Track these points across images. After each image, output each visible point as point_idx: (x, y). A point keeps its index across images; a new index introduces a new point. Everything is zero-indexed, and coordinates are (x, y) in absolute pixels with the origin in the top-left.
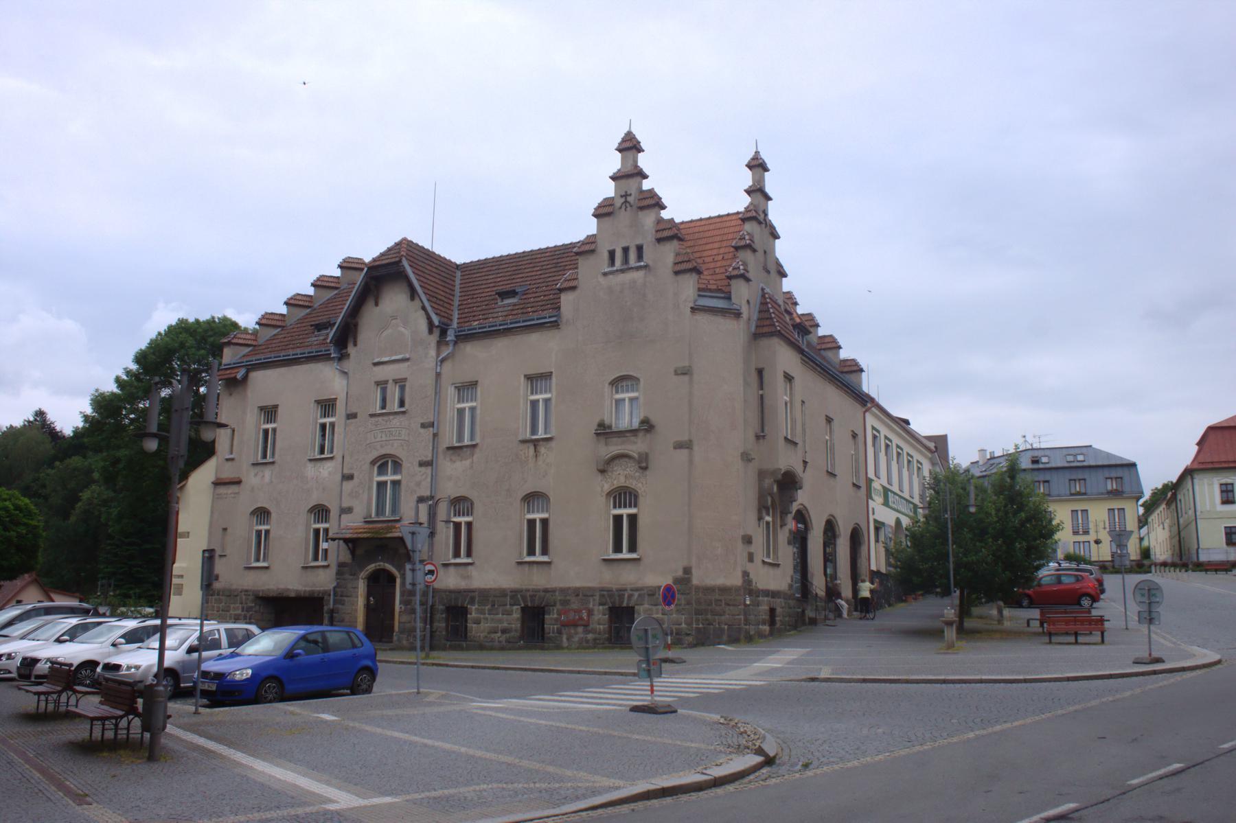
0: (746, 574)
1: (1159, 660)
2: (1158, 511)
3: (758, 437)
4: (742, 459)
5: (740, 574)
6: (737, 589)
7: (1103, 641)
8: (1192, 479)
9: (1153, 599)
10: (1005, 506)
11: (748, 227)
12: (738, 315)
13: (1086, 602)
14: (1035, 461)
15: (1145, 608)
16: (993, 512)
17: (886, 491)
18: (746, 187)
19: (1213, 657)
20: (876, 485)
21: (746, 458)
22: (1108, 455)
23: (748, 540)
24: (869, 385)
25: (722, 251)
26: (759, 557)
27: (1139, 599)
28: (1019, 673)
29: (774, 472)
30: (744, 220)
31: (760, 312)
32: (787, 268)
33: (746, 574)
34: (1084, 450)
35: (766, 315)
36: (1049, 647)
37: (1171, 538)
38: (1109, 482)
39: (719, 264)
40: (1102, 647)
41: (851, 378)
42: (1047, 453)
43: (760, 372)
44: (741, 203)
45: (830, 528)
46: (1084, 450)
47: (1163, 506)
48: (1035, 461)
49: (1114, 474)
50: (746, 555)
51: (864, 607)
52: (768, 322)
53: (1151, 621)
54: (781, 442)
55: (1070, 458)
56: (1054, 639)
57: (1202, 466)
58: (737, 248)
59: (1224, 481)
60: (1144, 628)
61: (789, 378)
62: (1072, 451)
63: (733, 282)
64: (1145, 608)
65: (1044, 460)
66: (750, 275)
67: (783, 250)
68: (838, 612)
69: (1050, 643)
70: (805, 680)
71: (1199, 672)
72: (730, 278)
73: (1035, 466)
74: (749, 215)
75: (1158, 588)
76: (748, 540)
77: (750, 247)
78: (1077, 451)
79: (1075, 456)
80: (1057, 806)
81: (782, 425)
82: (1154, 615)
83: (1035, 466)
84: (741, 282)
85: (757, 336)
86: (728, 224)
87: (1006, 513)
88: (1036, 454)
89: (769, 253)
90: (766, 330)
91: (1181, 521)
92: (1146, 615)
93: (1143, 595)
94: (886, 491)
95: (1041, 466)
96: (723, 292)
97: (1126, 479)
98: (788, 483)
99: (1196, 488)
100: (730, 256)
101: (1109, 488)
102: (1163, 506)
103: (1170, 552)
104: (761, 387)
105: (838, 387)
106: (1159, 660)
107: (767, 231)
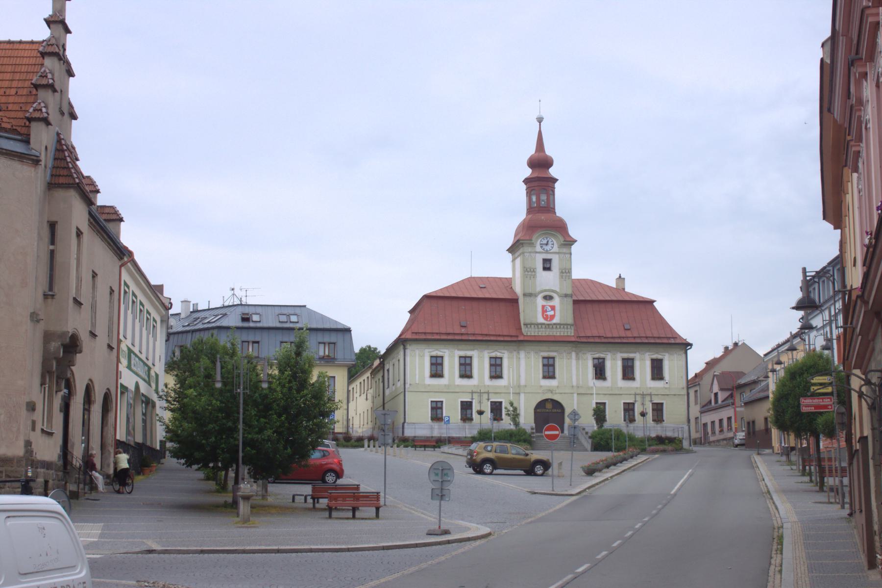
0: (28, 444)
1: (446, 532)
2: (361, 380)
3: (46, 296)
4: (32, 320)
5: (22, 443)
6: (19, 460)
7: (354, 517)
8: (405, 349)
9: (446, 478)
10: (290, 382)
11: (49, 62)
12: (36, 162)
13: (330, 478)
14: (246, 319)
15: (437, 486)
16: (279, 389)
17: (130, 351)
18: (46, 16)
19: (485, 530)
20: (123, 347)
21: (35, 318)
22: (323, 317)
23: (31, 407)
24: (127, 236)
25: (15, 84)
26: (39, 427)
27: (433, 477)
28: (338, 544)
29: (64, 334)
30: (43, 55)
31: (55, 159)
32: (77, 110)
33: (28, 444)
34: (298, 311)
35: (63, 164)
36: (330, 521)
37: (374, 410)
38: (322, 346)
39: (11, 99)
40: (376, 521)
41: (110, 226)
42: (259, 310)
43: (52, 226)
44: (43, 33)
45: (89, 390)
46: (298, 311)
47: (368, 374)
48: (246, 319)
49: (327, 338)
50: (29, 423)
51: (121, 478)
52: (65, 172)
53: (442, 497)
54: (71, 301)
55: (283, 318)
56: (334, 514)
57: (415, 337)
58: (36, 87)
59: (434, 353)
60: (437, 503)
61: (79, 234)
62: (285, 311)
63: (34, 125)
64: (438, 485)
65: (255, 318)
66: (51, 119)
67: (78, 91)
68: (93, 487)
69: (330, 517)
70: (141, 552)
71: (478, 543)
72: (30, 120)
73: (246, 324)
74: (50, 49)
75: (451, 469)
76: (31, 407)
77: (52, 87)
78: (290, 311)
79: (289, 316)
80: (876, 498)
81: (71, 282)
82: (445, 492)
83: (246, 324)
84: (41, 126)
85: (51, 186)
86: (21, 53)
87: (290, 389)
88: (246, 310)
89: (63, 92)
90: (62, 180)
91: (387, 392)
92: (438, 492)
93: (437, 474)
94: (130, 351)
95: (251, 325)
96: (19, 134)
97: (340, 344)
98: (72, 346)
99: (408, 359)
100: (25, 92)
101: (321, 353)
102: (368, 374)
103: (370, 425)
104: (53, 242)
105: (103, 239)
106: (446, 532)
107: (64, 67)
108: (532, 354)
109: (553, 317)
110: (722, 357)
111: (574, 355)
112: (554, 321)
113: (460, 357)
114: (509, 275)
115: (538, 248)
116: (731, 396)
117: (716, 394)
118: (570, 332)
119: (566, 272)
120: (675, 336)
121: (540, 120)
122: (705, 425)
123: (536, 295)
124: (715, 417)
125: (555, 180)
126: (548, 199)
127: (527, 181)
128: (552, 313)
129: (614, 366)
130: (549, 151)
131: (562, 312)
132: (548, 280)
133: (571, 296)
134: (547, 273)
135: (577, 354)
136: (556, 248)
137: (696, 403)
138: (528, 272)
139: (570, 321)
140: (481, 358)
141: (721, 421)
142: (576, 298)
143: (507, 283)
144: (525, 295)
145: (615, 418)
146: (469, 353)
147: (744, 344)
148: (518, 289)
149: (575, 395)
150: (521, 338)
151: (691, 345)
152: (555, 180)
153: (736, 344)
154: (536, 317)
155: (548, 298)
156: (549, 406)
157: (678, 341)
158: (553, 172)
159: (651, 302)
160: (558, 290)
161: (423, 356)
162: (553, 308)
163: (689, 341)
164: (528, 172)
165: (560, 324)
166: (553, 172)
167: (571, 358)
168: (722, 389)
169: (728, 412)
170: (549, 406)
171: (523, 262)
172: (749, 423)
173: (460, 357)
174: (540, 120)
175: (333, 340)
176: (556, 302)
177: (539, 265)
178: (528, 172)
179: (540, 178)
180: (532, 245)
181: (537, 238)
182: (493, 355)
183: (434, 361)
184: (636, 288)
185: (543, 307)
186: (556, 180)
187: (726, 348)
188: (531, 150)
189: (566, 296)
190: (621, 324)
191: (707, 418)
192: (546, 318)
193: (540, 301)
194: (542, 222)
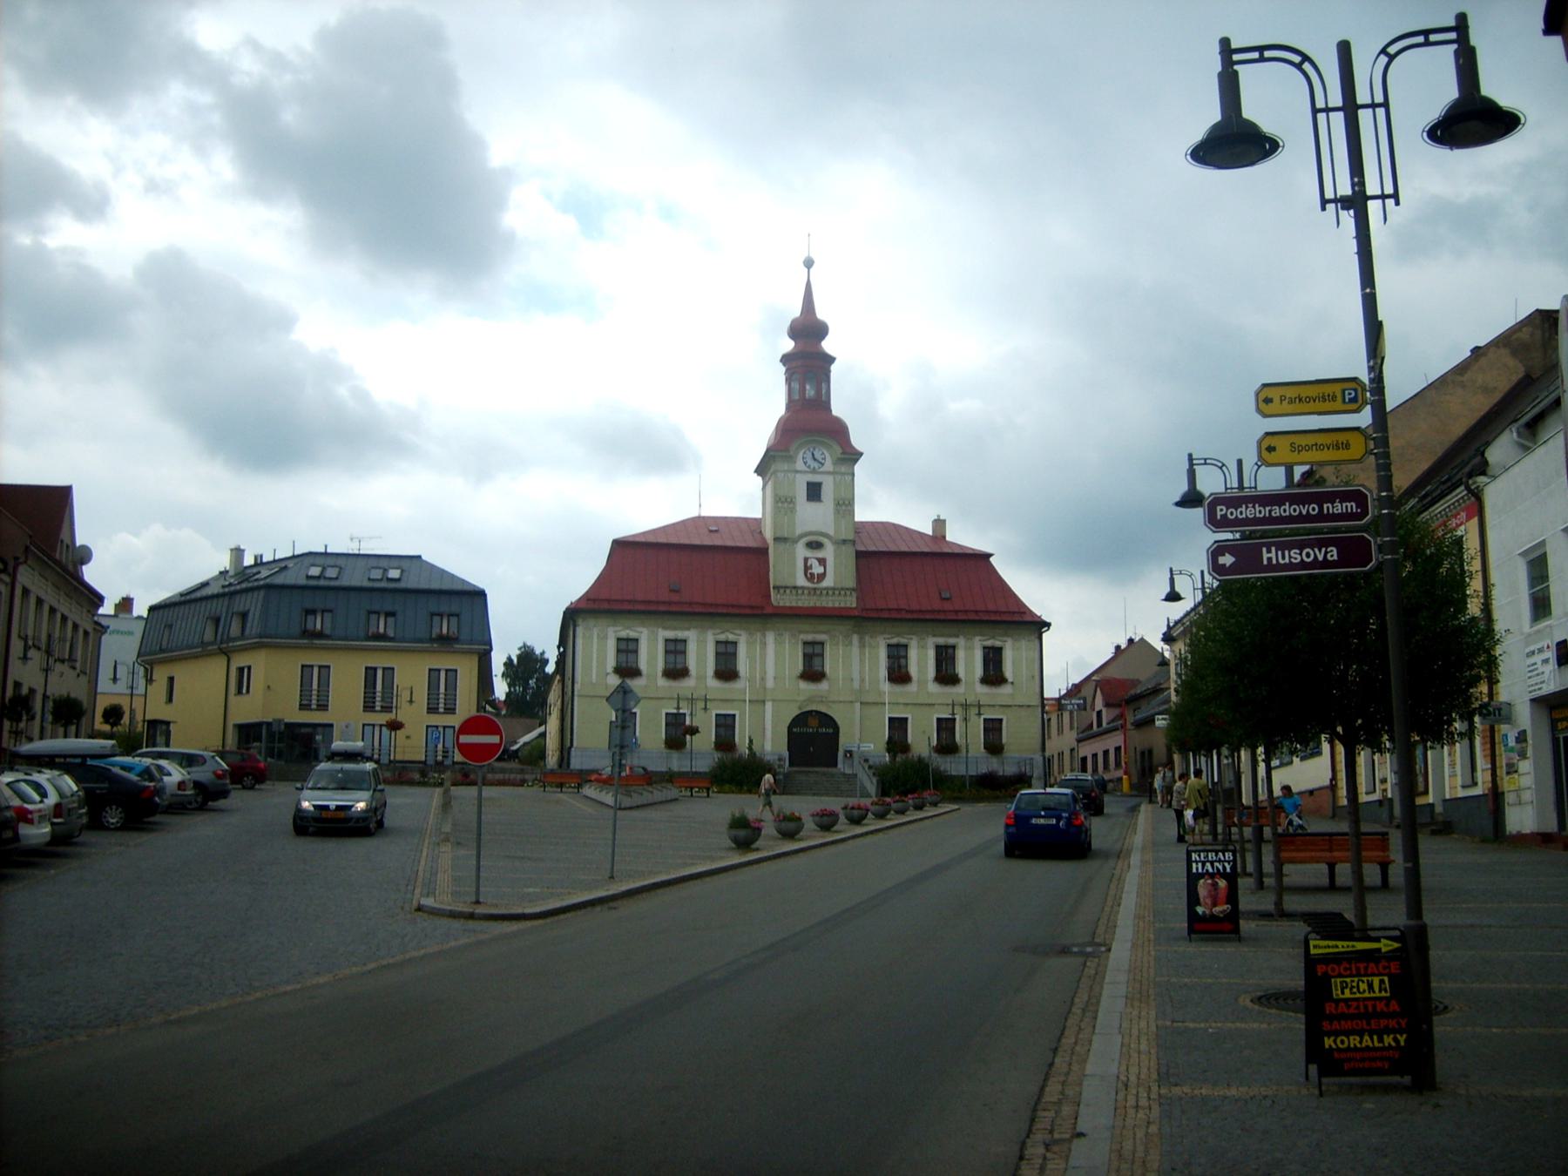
55: (376, 574)
59: (624, 634)
62: (384, 563)
79: (385, 570)
108: (787, 636)
109: (822, 577)
110: (1112, 659)
111: (855, 638)
112: (828, 582)
113: (667, 641)
114: (759, 515)
115: (800, 465)
116: (1122, 716)
117: (1099, 713)
118: (851, 602)
119: (845, 505)
120: (1022, 609)
121: (809, 263)
122: (1084, 759)
123: (796, 541)
124: (1097, 747)
125: (831, 360)
126: (819, 391)
127: (785, 359)
128: (821, 570)
129: (922, 660)
130: (821, 314)
131: (837, 571)
132: (815, 517)
133: (854, 542)
134: (813, 506)
135: (861, 640)
136: (828, 466)
137: (1071, 728)
138: (781, 503)
139: (850, 582)
140: (701, 643)
141: (1106, 753)
142: (862, 549)
143: (753, 525)
144: (776, 539)
145: (922, 739)
146: (680, 634)
147: (1142, 640)
148: (768, 534)
149: (858, 705)
150: (768, 610)
151: (1048, 625)
152: (831, 360)
153: (1131, 641)
154: (794, 576)
155: (815, 545)
156: (813, 722)
157: (1028, 619)
158: (828, 345)
159: (986, 556)
160: (831, 533)
161: (606, 637)
162: (822, 562)
163: (1046, 618)
164: (788, 345)
165: (834, 589)
166: (828, 345)
167: (851, 643)
168: (1107, 705)
169: (1116, 740)
170: (813, 722)
171: (775, 488)
172: (1143, 753)
173: (667, 641)
174: (809, 263)
175: (454, 609)
176: (828, 552)
177: (802, 492)
178: (788, 345)
179: (808, 359)
180: (791, 459)
181: (798, 449)
182: (722, 637)
183: (623, 646)
184: (961, 536)
185: (806, 560)
186: (1048, 625)
187: (1118, 648)
188: (796, 311)
189: (844, 541)
190: (941, 595)
191: (1086, 750)
192: (810, 577)
193: (801, 551)
194: (811, 430)
